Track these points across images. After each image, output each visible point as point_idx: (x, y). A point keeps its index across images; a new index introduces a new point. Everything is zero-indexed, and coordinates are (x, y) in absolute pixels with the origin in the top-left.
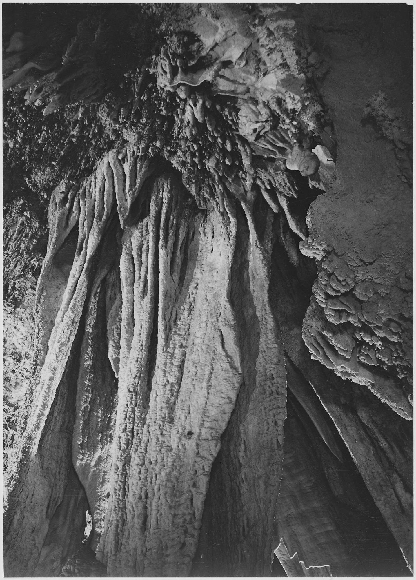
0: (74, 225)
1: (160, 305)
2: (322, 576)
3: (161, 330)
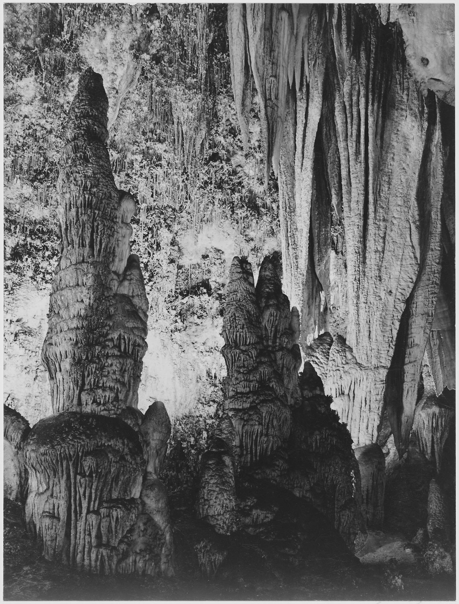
0: (316, 130)
1: (371, 178)
2: (4, 551)
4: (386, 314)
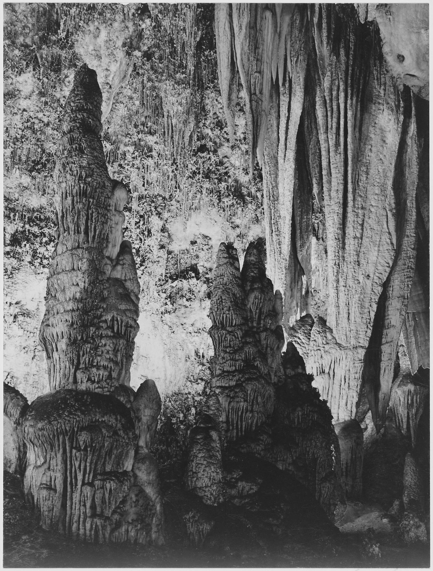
1: (350, 169)
3: (351, 193)
4: (364, 297)
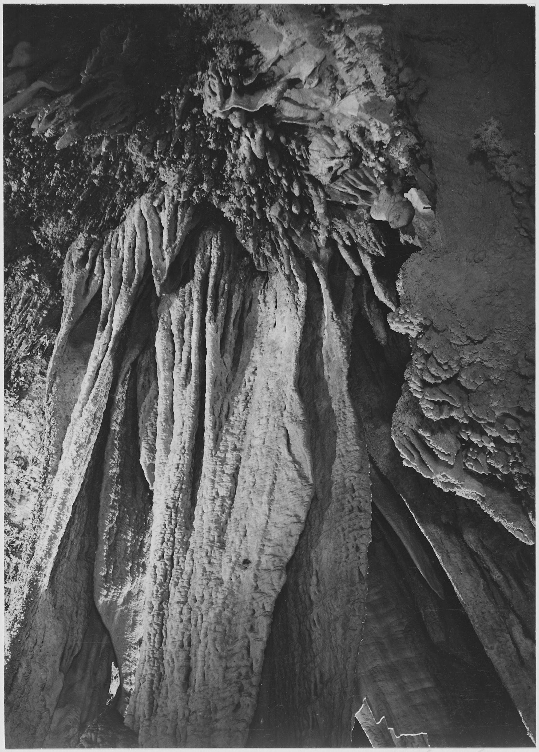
1: (208, 396)
3: (209, 428)
4: (234, 614)
